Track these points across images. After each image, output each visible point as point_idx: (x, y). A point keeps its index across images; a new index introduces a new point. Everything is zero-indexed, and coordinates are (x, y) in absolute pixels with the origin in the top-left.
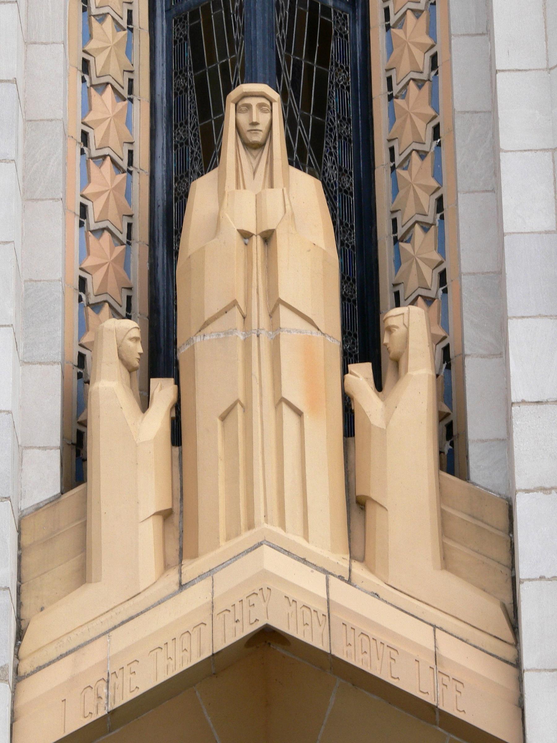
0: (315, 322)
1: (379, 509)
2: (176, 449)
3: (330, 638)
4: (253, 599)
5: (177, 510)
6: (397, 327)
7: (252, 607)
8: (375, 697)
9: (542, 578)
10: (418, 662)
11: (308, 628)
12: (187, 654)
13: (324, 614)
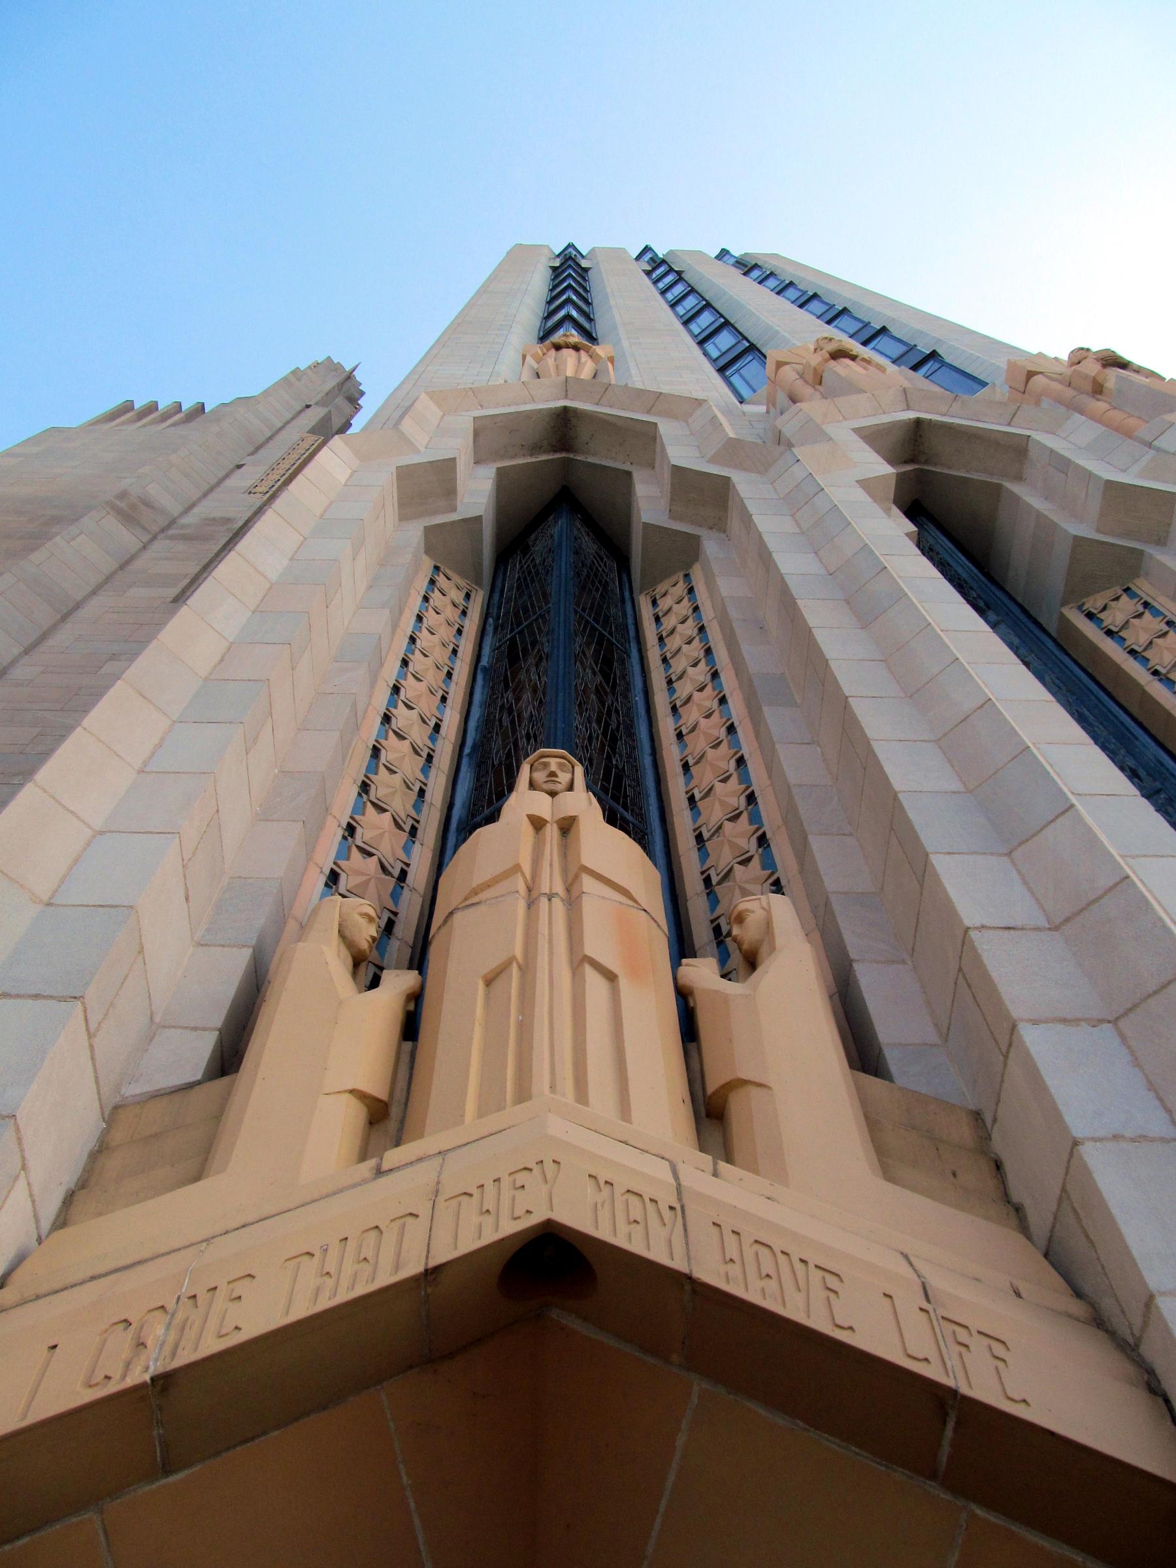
0: (634, 894)
1: (754, 1091)
2: (408, 1045)
3: (687, 1244)
4: (522, 1178)
5: (395, 1111)
6: (753, 912)
7: (520, 1191)
8: (781, 1421)
9: (1116, 1137)
10: (890, 1297)
11: (639, 1228)
12: (367, 1268)
13: (673, 1205)
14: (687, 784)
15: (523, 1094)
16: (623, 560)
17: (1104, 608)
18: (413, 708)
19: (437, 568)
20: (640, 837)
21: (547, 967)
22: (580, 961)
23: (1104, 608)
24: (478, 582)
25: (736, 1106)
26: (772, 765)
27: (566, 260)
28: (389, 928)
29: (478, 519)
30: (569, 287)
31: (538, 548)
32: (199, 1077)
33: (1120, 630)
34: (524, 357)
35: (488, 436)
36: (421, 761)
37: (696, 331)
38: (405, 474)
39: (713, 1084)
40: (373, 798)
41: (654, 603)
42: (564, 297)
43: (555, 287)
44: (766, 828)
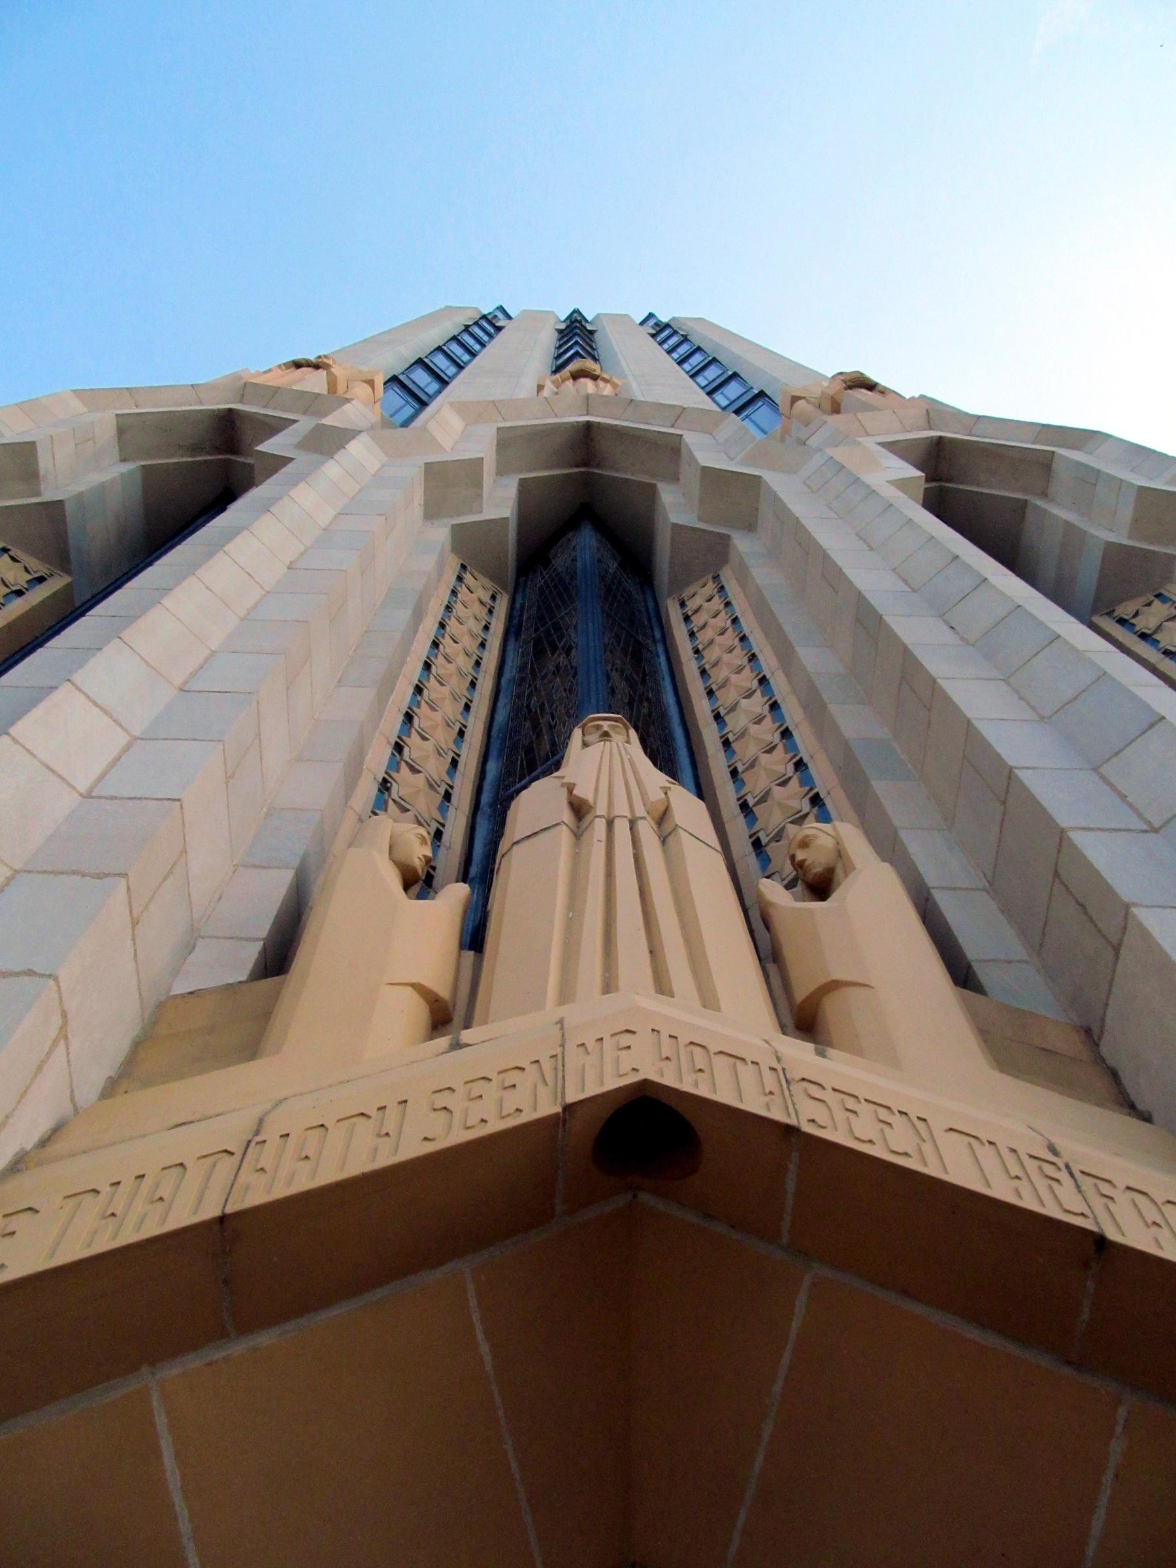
1: (855, 991)
17: (1136, 614)
18: (427, 739)
19: (463, 567)
23: (1136, 614)
24: (504, 587)
25: (831, 1007)
27: (572, 323)
29: (507, 518)
31: (560, 561)
32: (244, 978)
33: (1155, 632)
37: (704, 383)
41: (683, 604)
43: (560, 347)
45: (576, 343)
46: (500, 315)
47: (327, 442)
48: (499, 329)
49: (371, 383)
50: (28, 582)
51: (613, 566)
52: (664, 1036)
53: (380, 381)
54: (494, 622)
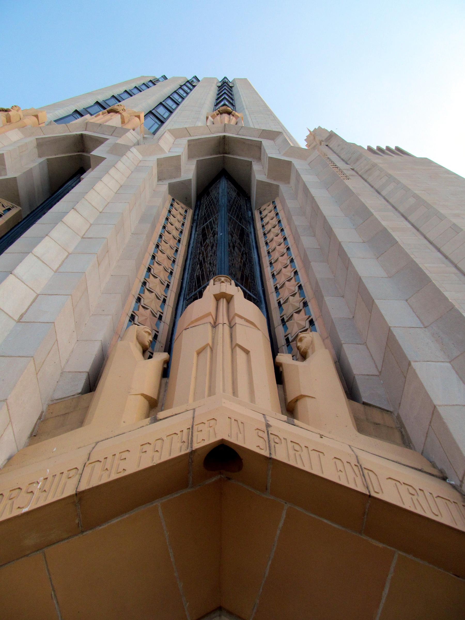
1: (307, 399)
14: (274, 283)
15: (211, 392)
16: (248, 198)
18: (157, 278)
19: (173, 199)
20: (257, 302)
21: (221, 361)
22: (234, 346)
25: (300, 406)
26: (289, 220)
28: (156, 337)
29: (190, 180)
30: (225, 98)
31: (213, 193)
34: (207, 118)
35: (194, 146)
36: (160, 302)
38: (160, 162)
39: (290, 398)
40: (156, 261)
41: (261, 213)
42: (223, 97)
43: (219, 90)
44: (307, 299)
45: (225, 89)
46: (194, 80)
47: (120, 151)
48: (194, 86)
49: (139, 117)
50: (4, 211)
51: (234, 194)
52: (233, 420)
53: (142, 116)
54: (186, 222)
